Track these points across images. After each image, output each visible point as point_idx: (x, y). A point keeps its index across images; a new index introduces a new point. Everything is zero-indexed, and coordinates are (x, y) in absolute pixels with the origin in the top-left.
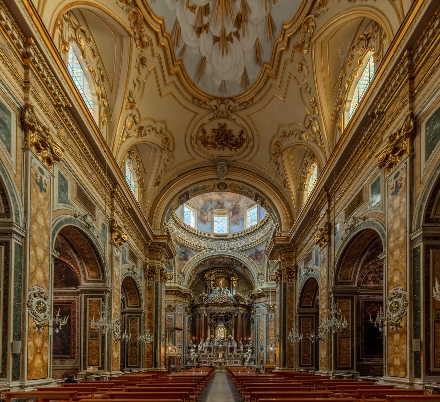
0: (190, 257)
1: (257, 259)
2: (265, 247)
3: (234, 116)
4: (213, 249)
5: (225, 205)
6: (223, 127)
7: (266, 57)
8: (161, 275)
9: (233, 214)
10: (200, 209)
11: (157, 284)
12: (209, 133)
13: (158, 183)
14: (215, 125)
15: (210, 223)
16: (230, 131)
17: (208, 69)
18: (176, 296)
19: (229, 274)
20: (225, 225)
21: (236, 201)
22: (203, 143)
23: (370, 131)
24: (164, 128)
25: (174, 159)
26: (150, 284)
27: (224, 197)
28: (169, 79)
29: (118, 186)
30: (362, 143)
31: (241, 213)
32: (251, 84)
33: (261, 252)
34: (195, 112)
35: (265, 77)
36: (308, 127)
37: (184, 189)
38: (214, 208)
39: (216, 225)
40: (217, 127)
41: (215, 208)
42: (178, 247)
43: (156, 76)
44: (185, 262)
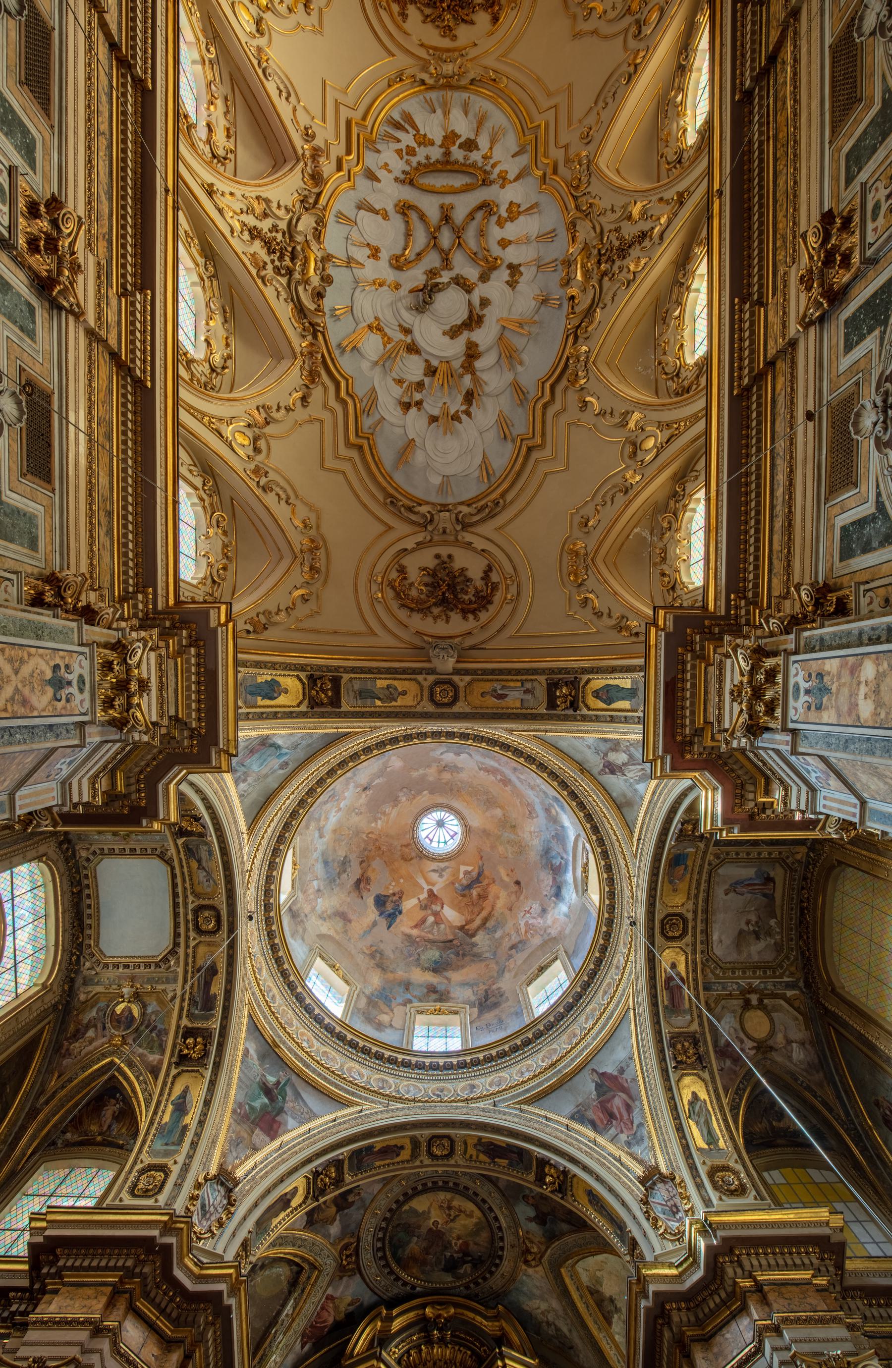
0: (291, 1123)
1: (611, 1116)
3: (468, 537)
4: (400, 1100)
5: (452, 995)
6: (444, 563)
14: (427, 558)
16: (463, 570)
17: (419, 457)
18: (121, 1306)
19: (476, 1332)
27: (449, 979)
28: (343, 451)
33: (622, 1071)
34: (386, 524)
35: (524, 450)
40: (431, 563)
42: (252, 1052)
43: (322, 433)
44: (259, 1136)
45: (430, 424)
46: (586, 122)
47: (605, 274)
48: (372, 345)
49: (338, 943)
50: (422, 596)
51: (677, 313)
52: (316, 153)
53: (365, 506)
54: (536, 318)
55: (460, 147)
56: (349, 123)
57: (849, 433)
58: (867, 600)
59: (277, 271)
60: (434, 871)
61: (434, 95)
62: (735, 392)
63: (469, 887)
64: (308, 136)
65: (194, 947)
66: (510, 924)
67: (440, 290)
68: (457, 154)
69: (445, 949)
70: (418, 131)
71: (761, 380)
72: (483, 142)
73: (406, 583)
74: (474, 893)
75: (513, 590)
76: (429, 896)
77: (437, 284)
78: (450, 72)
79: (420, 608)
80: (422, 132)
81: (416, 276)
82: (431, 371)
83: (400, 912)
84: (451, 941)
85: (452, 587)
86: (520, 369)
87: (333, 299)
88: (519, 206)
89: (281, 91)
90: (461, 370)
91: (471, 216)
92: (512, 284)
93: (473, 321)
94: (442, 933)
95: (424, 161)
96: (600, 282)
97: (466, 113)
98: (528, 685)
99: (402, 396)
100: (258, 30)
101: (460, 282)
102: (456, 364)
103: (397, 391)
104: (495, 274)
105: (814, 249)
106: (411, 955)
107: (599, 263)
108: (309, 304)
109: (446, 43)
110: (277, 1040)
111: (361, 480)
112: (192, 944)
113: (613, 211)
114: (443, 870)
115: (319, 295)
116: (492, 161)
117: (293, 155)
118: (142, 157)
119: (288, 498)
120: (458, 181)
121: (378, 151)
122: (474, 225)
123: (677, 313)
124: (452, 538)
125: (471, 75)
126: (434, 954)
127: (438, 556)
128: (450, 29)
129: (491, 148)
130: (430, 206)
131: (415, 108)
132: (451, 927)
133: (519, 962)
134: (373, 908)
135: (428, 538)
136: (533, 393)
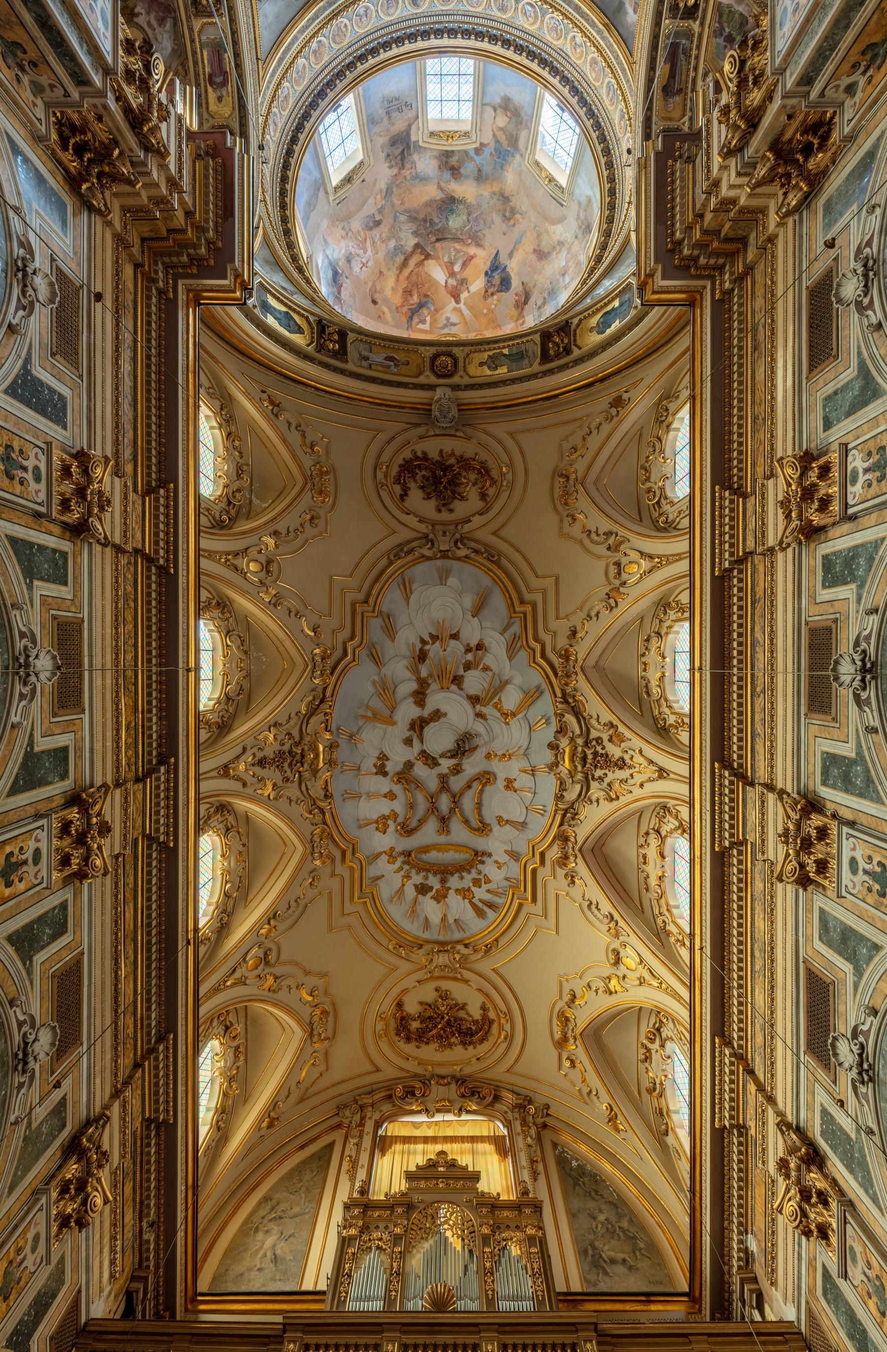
2: (261, 21)
3: (422, 528)
5: (435, 163)
6: (445, 504)
7: (376, 624)
8: (752, 120)
9: (408, 135)
10: (518, 157)
11: (807, 80)
12: (472, 493)
13: (618, 403)
14: (460, 509)
15: (486, 101)
16: (428, 497)
17: (468, 601)
20: (432, 89)
21: (400, 179)
22: (488, 471)
23: (150, 737)
24: (566, 524)
25: (561, 445)
26: (845, 81)
27: (440, 188)
28: (538, 598)
29: (717, 573)
30: (150, 711)
31: (381, 141)
32: (395, 584)
34: (498, 537)
35: (371, 601)
36: (269, 562)
37: (551, 372)
38: (472, 153)
39: (467, 90)
40: (457, 505)
41: (466, 153)
42: (630, 10)
43: (557, 608)
45: (458, 632)
46: (315, 892)
47: (297, 744)
48: (511, 698)
49: (546, 218)
50: (464, 473)
51: (228, 886)
52: (564, 859)
53: (518, 550)
54: (361, 722)
55: (431, 888)
56: (534, 900)
57: (61, 1027)
58: (39, 876)
59: (599, 740)
60: (455, 325)
61: (457, 936)
62: (173, 760)
63: (421, 306)
64: (572, 878)
65: (684, 115)
66: (381, 254)
67: (450, 751)
68: (434, 882)
69: (444, 229)
70: (471, 902)
71: (148, 769)
72: (410, 892)
73: (480, 485)
74: (415, 299)
75: (380, 475)
76: (459, 296)
77: (453, 757)
78: (441, 955)
79: (465, 463)
80: (467, 901)
81: (472, 766)
82: (457, 680)
83: (486, 273)
84: (438, 240)
85: (437, 481)
86: (376, 678)
87: (548, 733)
88: (377, 829)
89: (597, 907)
90: (430, 682)
91: (421, 822)
92: (383, 757)
93: (419, 726)
94: (447, 250)
95: (464, 874)
96: (301, 738)
97: (426, 919)
98: (364, 364)
99: (483, 655)
100: (618, 953)
101: (430, 760)
102: (434, 686)
103: (488, 660)
104: (399, 768)
105: (97, 1190)
106: (476, 220)
107: (303, 756)
108: (570, 719)
109: (445, 985)
110: (606, 34)
111: (520, 573)
112: (686, 118)
113: (290, 988)
114: (446, 326)
115: (562, 730)
116: (402, 873)
117: (585, 854)
118: (723, 957)
119: (589, 536)
120: (433, 856)
121: (506, 879)
122: (418, 816)
123: (228, 886)
124: (437, 527)
125: (421, 952)
126: (455, 222)
127: (451, 511)
128: (441, 997)
129: (403, 885)
130: (459, 832)
131: (475, 924)
132: (437, 258)
133: (371, 200)
134: (512, 275)
135: (459, 527)
136: (363, 653)
